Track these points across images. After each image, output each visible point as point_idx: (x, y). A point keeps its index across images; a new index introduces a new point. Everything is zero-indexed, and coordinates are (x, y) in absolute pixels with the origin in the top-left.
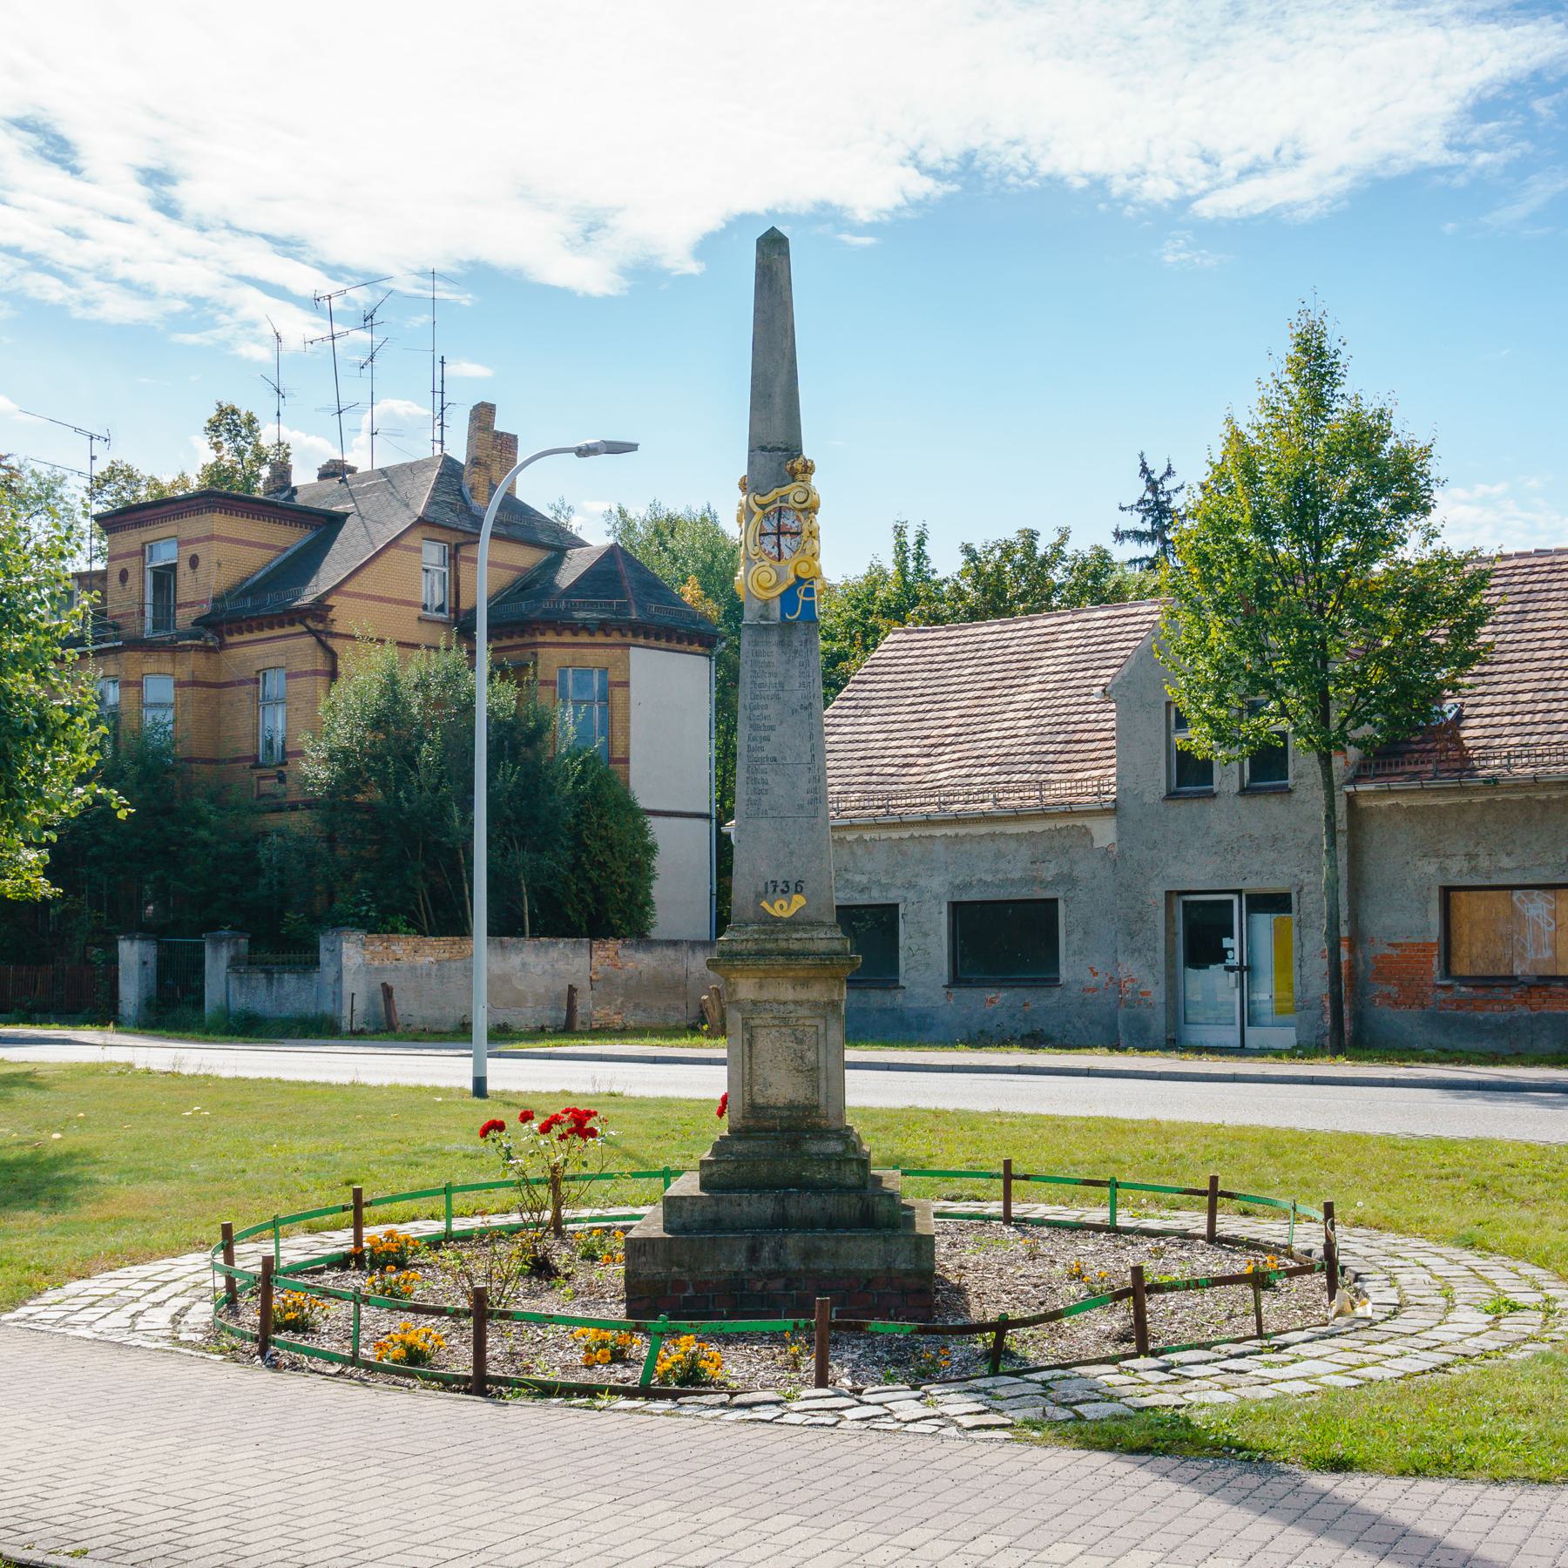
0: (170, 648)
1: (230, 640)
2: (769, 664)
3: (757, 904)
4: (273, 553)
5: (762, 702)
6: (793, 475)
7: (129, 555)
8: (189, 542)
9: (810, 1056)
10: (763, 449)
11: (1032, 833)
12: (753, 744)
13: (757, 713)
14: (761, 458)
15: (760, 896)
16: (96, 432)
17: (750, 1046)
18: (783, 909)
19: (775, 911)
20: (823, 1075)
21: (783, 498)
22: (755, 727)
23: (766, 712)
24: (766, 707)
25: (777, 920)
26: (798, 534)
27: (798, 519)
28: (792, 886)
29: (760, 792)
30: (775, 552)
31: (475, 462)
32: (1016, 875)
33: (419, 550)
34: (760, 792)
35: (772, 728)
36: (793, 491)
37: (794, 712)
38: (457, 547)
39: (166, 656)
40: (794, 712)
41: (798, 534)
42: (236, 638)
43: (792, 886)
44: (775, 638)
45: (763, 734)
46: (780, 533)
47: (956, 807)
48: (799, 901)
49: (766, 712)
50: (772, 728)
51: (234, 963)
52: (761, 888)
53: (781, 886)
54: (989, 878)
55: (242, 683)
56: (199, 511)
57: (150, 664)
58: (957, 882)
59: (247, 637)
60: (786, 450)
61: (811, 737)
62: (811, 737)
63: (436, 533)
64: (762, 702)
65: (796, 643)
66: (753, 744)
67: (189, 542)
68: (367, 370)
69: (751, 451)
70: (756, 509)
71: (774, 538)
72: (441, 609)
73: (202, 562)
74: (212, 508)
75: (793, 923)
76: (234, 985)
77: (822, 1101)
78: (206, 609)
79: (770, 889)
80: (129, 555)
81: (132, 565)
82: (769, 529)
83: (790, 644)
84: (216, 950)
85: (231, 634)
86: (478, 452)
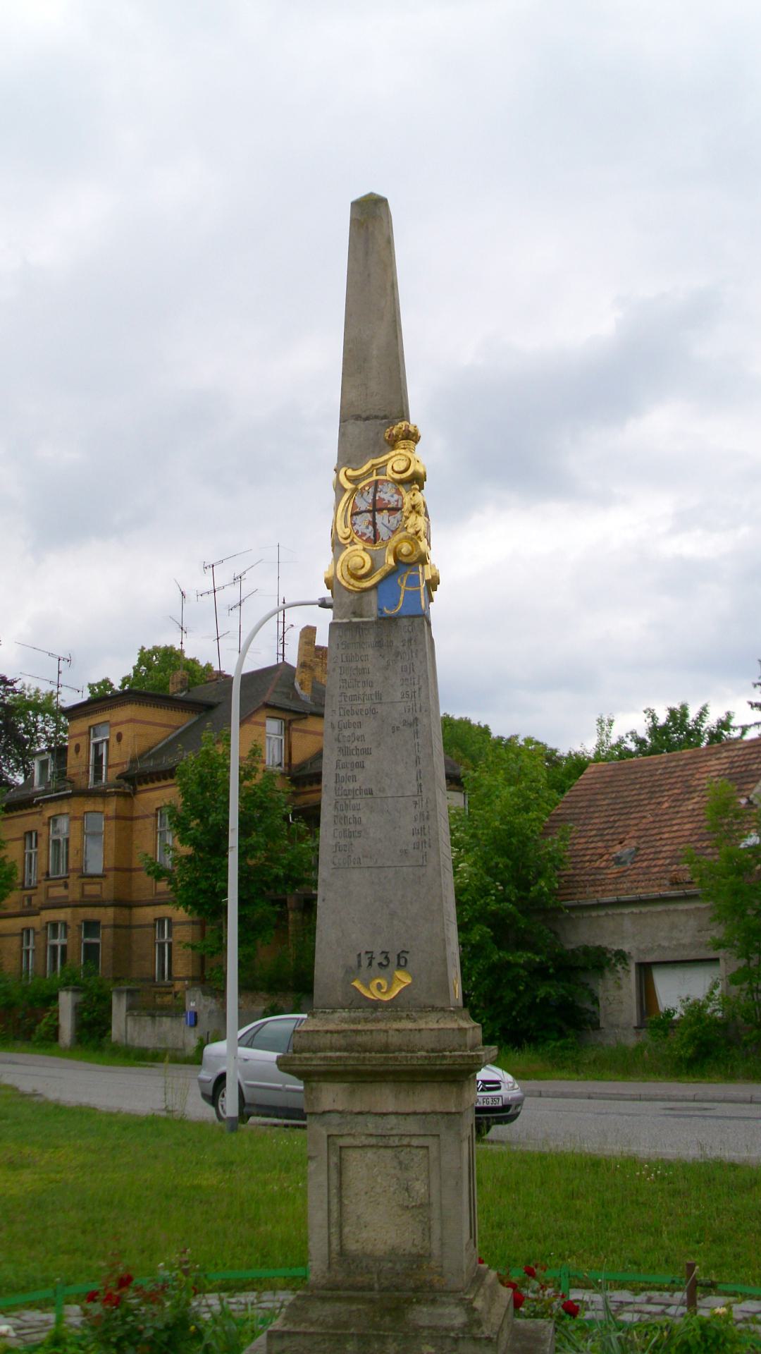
0: (101, 794)
1: (140, 788)
2: (363, 671)
3: (347, 983)
4: (169, 730)
5: (355, 719)
6: (392, 443)
7: (80, 735)
8: (117, 724)
9: (420, 1188)
10: (358, 418)
11: (698, 909)
12: (342, 773)
13: (347, 733)
14: (355, 428)
15: (352, 972)
16: (62, 655)
17: (340, 1173)
18: (379, 990)
19: (372, 993)
20: (435, 1213)
21: (380, 469)
22: (344, 751)
23: (359, 732)
24: (360, 725)
25: (376, 1005)
26: (396, 509)
27: (399, 493)
28: (393, 959)
29: (350, 835)
30: (369, 532)
31: (303, 665)
32: (686, 941)
33: (264, 725)
34: (350, 835)
35: (367, 752)
36: (395, 461)
37: (395, 729)
38: (290, 722)
39: (100, 800)
40: (395, 729)
41: (396, 509)
42: (144, 787)
43: (393, 959)
44: (371, 638)
45: (355, 759)
46: (376, 508)
47: (640, 890)
48: (403, 979)
49: (359, 732)
50: (367, 752)
51: (130, 1008)
52: (353, 961)
53: (379, 959)
54: (666, 944)
55: (147, 816)
56: (123, 704)
57: (89, 805)
58: (642, 947)
59: (151, 786)
60: (385, 417)
61: (417, 761)
62: (417, 761)
63: (275, 713)
64: (355, 719)
65: (397, 643)
66: (342, 773)
67: (117, 724)
68: (236, 611)
69: (343, 420)
70: (348, 485)
71: (368, 516)
72: (280, 765)
73: (124, 737)
74: (130, 702)
75: (395, 1007)
76: (130, 1023)
77: (435, 1247)
78: (126, 767)
79: (365, 962)
80: (80, 735)
81: (82, 741)
82: (363, 505)
83: (390, 645)
84: (119, 999)
85: (140, 784)
86: (308, 660)
